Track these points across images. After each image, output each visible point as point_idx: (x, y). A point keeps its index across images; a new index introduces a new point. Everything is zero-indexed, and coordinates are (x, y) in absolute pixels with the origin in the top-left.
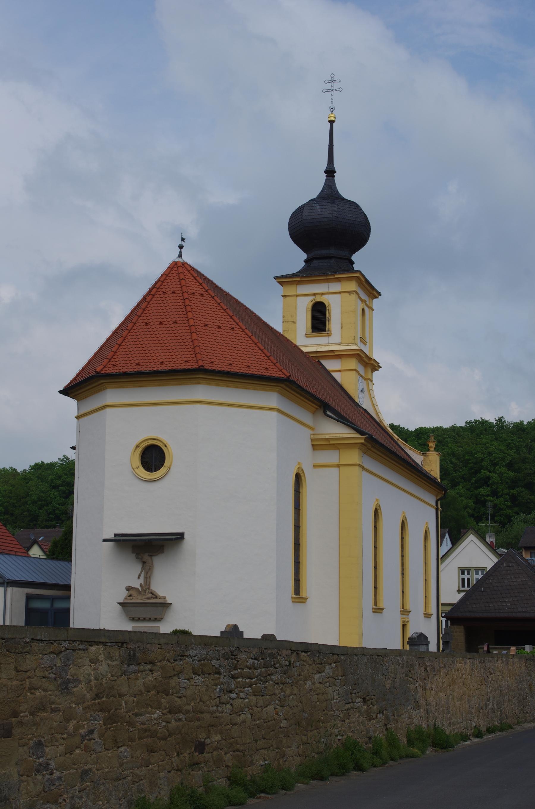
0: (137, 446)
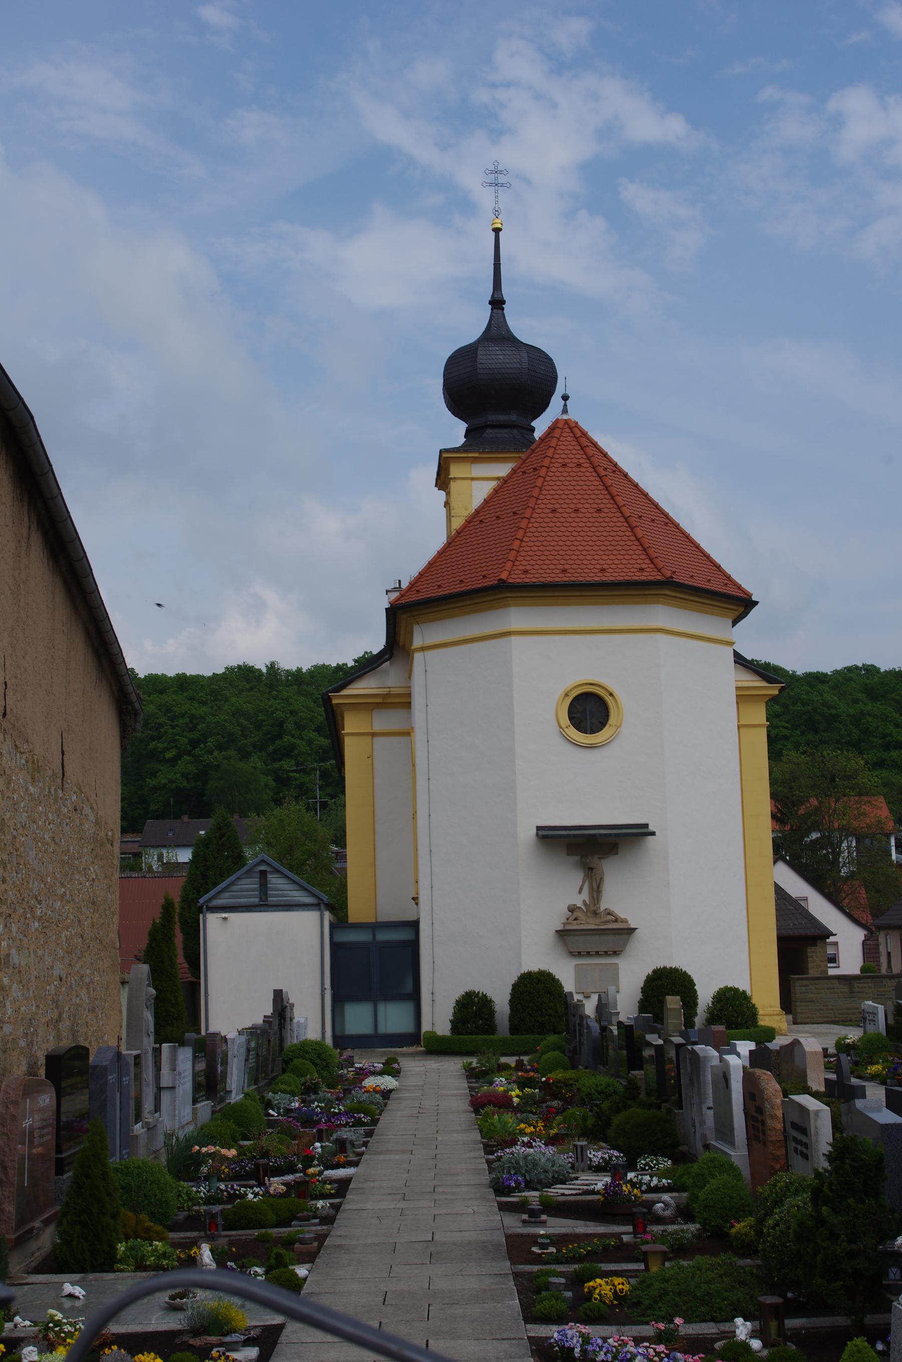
0: (567, 695)
